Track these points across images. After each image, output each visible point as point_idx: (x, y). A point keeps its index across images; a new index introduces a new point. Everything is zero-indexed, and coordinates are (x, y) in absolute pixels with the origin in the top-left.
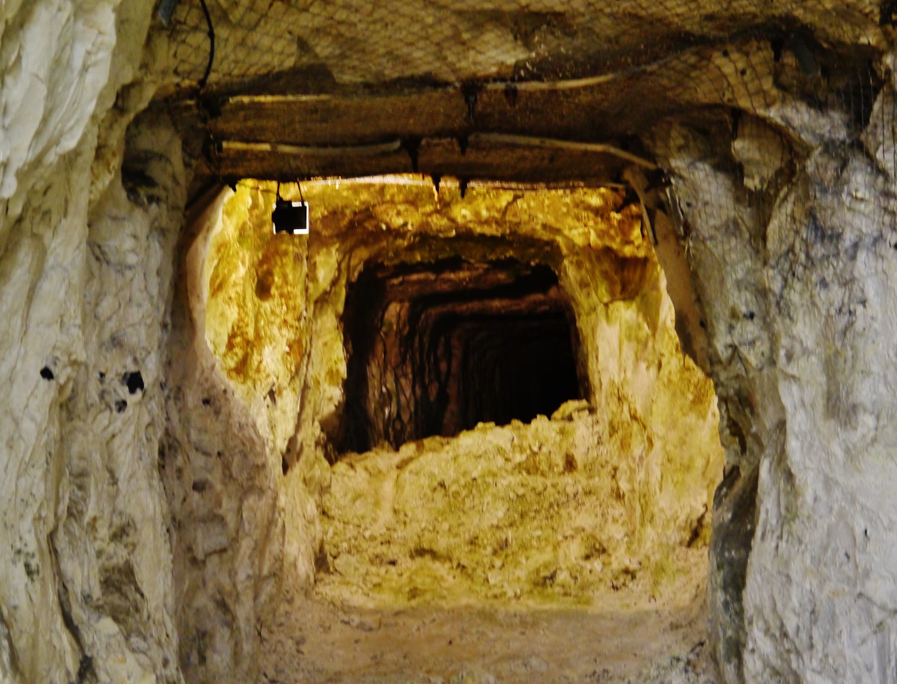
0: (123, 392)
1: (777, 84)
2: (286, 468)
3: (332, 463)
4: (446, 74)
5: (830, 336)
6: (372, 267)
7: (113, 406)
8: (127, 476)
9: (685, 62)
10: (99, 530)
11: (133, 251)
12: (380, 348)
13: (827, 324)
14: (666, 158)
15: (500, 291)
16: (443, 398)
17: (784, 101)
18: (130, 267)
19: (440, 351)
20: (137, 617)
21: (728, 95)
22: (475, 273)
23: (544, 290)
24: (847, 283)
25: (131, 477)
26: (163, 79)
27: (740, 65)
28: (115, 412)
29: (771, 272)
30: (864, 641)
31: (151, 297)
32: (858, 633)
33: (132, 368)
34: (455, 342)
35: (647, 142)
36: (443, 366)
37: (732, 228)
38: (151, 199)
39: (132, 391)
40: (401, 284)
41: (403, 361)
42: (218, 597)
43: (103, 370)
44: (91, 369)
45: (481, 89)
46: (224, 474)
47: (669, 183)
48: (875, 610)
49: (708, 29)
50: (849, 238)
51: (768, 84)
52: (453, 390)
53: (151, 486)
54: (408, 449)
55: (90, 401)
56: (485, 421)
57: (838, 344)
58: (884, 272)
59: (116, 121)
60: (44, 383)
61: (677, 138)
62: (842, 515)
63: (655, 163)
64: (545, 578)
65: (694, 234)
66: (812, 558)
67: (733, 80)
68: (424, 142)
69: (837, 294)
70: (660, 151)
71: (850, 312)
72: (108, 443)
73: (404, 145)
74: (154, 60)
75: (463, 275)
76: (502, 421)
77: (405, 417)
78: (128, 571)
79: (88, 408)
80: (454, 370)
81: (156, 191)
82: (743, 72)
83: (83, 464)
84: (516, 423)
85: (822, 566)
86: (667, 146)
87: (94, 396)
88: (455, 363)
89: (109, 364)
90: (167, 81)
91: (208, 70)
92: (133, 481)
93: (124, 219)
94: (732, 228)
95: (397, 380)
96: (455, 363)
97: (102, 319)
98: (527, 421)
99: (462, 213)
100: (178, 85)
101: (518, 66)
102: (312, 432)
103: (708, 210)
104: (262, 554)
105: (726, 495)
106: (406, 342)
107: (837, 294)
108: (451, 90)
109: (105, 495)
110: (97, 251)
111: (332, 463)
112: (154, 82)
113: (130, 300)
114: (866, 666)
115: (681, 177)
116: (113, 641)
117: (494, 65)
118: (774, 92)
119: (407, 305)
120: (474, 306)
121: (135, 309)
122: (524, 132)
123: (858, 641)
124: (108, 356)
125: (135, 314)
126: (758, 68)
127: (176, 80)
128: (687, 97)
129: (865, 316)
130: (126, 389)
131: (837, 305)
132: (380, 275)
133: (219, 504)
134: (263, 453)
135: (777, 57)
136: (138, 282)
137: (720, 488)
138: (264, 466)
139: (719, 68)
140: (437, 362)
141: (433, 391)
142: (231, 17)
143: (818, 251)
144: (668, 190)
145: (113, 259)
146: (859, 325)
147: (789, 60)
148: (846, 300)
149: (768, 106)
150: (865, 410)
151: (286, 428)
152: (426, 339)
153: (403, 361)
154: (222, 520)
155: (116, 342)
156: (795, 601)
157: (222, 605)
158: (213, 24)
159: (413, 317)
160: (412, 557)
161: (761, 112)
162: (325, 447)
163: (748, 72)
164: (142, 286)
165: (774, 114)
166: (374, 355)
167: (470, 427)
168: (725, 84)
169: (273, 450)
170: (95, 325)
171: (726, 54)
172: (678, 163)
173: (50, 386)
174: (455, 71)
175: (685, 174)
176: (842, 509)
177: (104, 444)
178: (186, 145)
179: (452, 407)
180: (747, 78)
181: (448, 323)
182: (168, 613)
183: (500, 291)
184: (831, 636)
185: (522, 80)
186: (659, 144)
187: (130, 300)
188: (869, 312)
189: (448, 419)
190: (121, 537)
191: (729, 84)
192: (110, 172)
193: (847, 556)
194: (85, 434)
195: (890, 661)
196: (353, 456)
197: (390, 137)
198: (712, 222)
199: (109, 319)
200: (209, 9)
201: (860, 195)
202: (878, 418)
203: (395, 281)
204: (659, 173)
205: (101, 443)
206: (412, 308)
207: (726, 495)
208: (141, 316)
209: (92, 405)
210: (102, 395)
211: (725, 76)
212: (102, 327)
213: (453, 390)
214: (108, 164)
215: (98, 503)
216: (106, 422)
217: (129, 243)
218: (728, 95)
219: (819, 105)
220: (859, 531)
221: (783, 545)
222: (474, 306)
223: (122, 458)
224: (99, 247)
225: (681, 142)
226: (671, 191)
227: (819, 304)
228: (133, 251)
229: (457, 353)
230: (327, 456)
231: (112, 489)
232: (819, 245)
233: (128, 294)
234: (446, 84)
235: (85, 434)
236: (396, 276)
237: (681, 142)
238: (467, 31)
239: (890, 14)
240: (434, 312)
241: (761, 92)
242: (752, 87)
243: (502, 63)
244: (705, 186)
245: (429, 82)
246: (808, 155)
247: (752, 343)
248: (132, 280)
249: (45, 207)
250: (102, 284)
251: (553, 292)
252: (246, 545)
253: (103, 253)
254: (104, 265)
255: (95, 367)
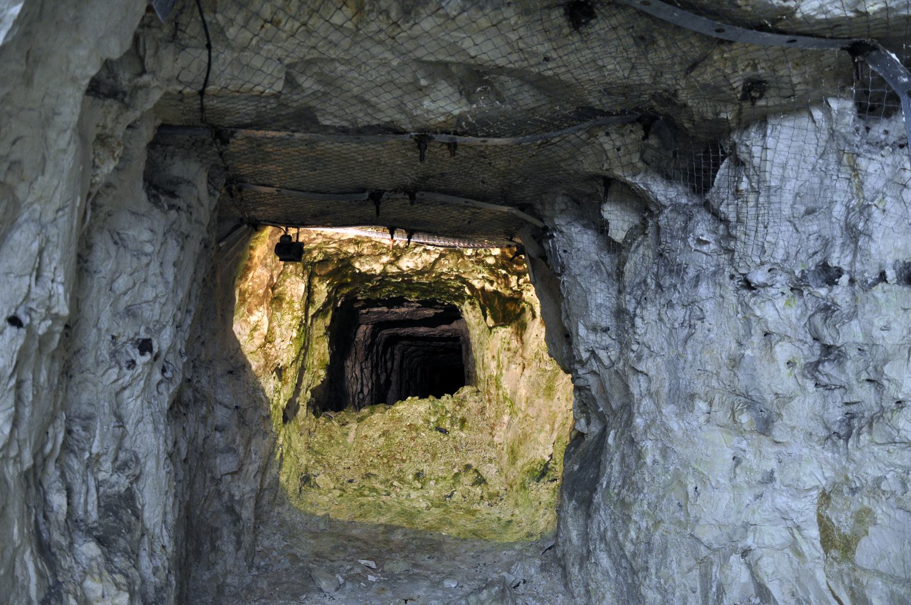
0: (134, 353)
1: (642, 159)
2: (286, 419)
3: (317, 416)
4: (406, 125)
5: (673, 343)
6: (350, 300)
7: (123, 364)
8: (135, 421)
9: (578, 137)
10: (103, 464)
11: (150, 242)
12: (353, 351)
13: (671, 333)
14: (552, 218)
15: (425, 322)
16: (388, 382)
17: (646, 172)
18: (146, 255)
19: (388, 356)
20: (128, 537)
21: (606, 166)
22: (411, 309)
23: (449, 322)
24: (689, 305)
25: (139, 422)
26: (168, 86)
27: (618, 144)
28: (125, 370)
29: (628, 297)
30: (690, 570)
31: (167, 282)
32: (685, 563)
33: (143, 335)
34: (396, 352)
35: (539, 207)
36: (389, 364)
37: (597, 266)
38: (171, 207)
39: (142, 353)
40: (367, 313)
41: (366, 359)
42: (229, 504)
43: (115, 334)
44: (103, 332)
45: (431, 139)
46: (239, 422)
47: (552, 236)
48: (702, 548)
49: (606, 103)
50: (691, 272)
51: (636, 159)
52: (394, 378)
53: (156, 429)
54: (365, 411)
55: (101, 358)
56: (413, 396)
57: (680, 349)
58: (722, 296)
59: (122, 114)
60: (10, 331)
61: (560, 202)
62: (677, 475)
63: (542, 221)
64: (446, 496)
65: (567, 272)
66: (649, 504)
67: (610, 155)
68: (384, 196)
69: (679, 313)
70: (547, 213)
71: (690, 326)
72: (117, 394)
73: (372, 196)
74: (161, 70)
75: (403, 310)
76: (423, 396)
77: (366, 391)
78: (129, 498)
79: (98, 363)
80: (395, 367)
81: (176, 201)
82: (619, 150)
83: (91, 410)
84: (431, 398)
85: (658, 511)
86: (553, 210)
87: (105, 354)
88: (396, 363)
89: (121, 330)
90: (170, 89)
91: (206, 84)
92: (141, 425)
93: (143, 215)
94: (597, 266)
95: (362, 370)
96: (396, 363)
97: (118, 292)
98: (439, 397)
99: (407, 263)
100: (180, 92)
101: (460, 118)
102: (305, 396)
103: (579, 254)
104: (264, 474)
105: (574, 452)
106: (369, 349)
107: (679, 313)
108: (406, 137)
109: (109, 436)
110: (116, 237)
111: (317, 416)
112: (161, 88)
113: (145, 281)
114: (691, 589)
115: (561, 232)
116: (94, 563)
117: (443, 114)
118: (640, 165)
119: (370, 326)
120: (409, 330)
121: (149, 289)
122: (454, 193)
123: (686, 570)
124: (121, 323)
125: (149, 294)
126: (629, 147)
127: (180, 88)
128: (575, 167)
129: (703, 328)
130: (137, 351)
131: (680, 320)
132: (356, 306)
133: (234, 441)
134: (268, 409)
135: (646, 137)
136: (154, 268)
137: (569, 447)
138: (269, 417)
139: (601, 144)
140: (386, 362)
141: (383, 378)
142: (227, 34)
143: (667, 281)
144: (550, 241)
145: (131, 245)
146: (699, 335)
147: (653, 141)
148: (687, 318)
149: (634, 175)
150: (701, 398)
151: (287, 391)
152: (380, 348)
153: (366, 359)
154: (234, 451)
155: (130, 312)
156: (633, 534)
157: (231, 510)
158: (211, 36)
159: (374, 335)
160: (363, 478)
161: (629, 179)
162: (314, 407)
163: (622, 149)
164: (158, 271)
165: (638, 181)
166: (349, 355)
167: (403, 398)
168: (605, 158)
169: (276, 407)
170: (110, 297)
171: (607, 134)
172: (560, 221)
173: (18, 334)
174: (413, 118)
175: (564, 229)
176: (676, 469)
177: (113, 395)
178: (211, 179)
179: (393, 387)
180: (621, 152)
181: (393, 340)
182: (166, 528)
183: (425, 322)
184: (663, 563)
185: (464, 134)
186: (547, 207)
187: (145, 281)
188: (706, 324)
189: (391, 394)
190: (124, 470)
191: (608, 158)
192: (114, 159)
193: (679, 505)
194: (95, 385)
195: (711, 586)
196: (331, 414)
197: (363, 190)
198: (583, 263)
199: (125, 293)
200: (208, 24)
201: (704, 238)
202: (711, 404)
203: (364, 311)
204: (546, 229)
205: (111, 394)
206: (374, 328)
207: (574, 452)
208: (154, 295)
209: (102, 362)
210: (113, 354)
211: (605, 151)
212: (117, 299)
213: (394, 378)
214: (114, 152)
215: (102, 442)
216: (115, 377)
217: (146, 235)
218: (606, 166)
219: (669, 178)
220: (690, 489)
221: (624, 492)
222: (409, 330)
223: (131, 406)
224: (118, 234)
225: (563, 207)
226: (553, 242)
227: (666, 320)
228: (150, 242)
229: (397, 357)
230: (314, 413)
231: (119, 431)
232: (667, 277)
233: (143, 277)
234: (404, 132)
235: (95, 385)
236: (363, 307)
237: (563, 207)
238: (424, 78)
239: (750, 91)
240: (386, 332)
241: (631, 164)
242: (624, 160)
243: (450, 113)
244: (579, 238)
245: (392, 129)
246: (661, 212)
247: (606, 348)
248: (148, 265)
249: (13, 157)
250: (118, 264)
251: (455, 325)
252: (252, 468)
253: (121, 239)
254: (122, 249)
255: (107, 330)
